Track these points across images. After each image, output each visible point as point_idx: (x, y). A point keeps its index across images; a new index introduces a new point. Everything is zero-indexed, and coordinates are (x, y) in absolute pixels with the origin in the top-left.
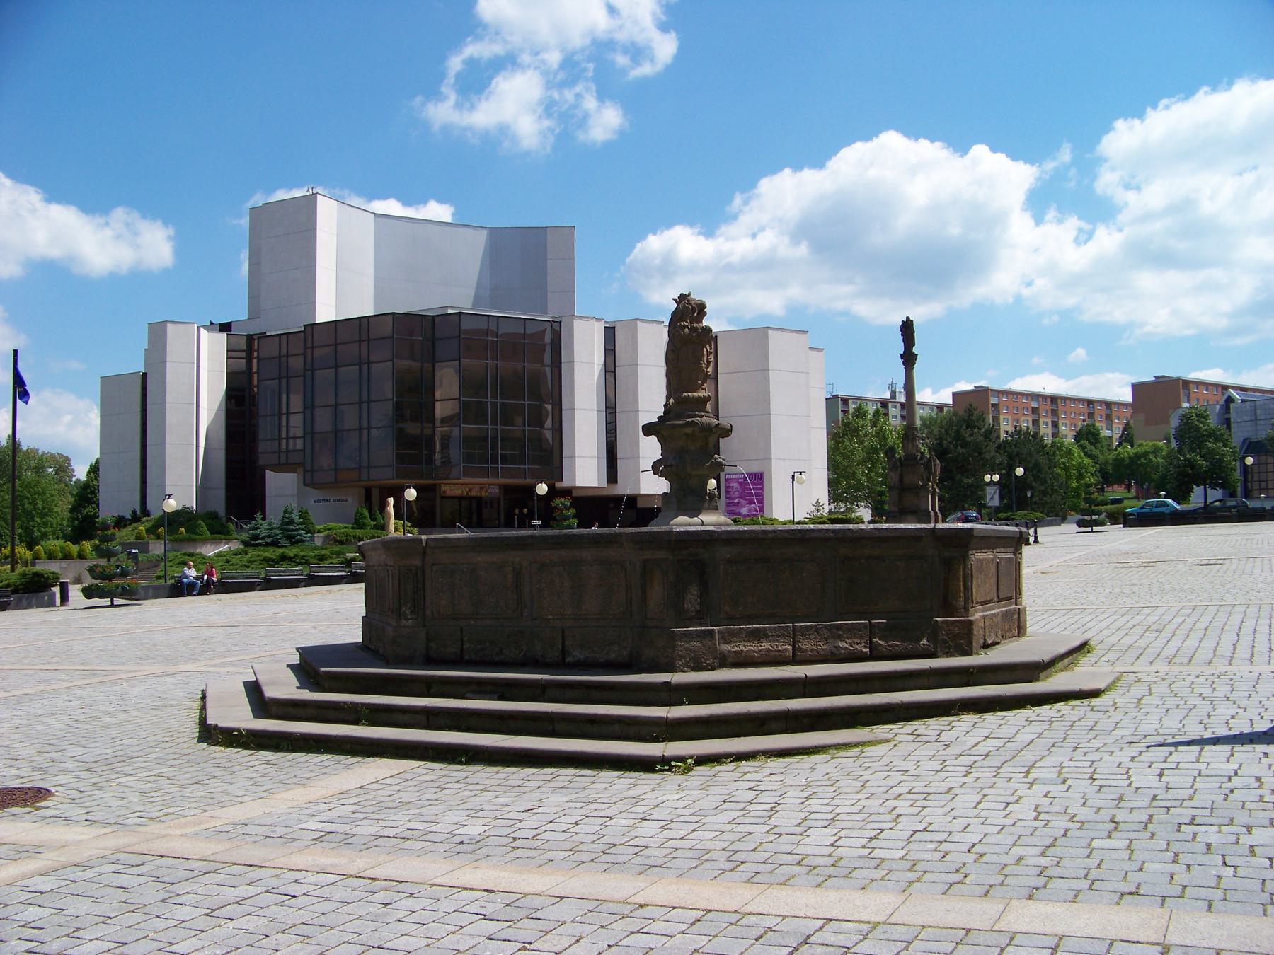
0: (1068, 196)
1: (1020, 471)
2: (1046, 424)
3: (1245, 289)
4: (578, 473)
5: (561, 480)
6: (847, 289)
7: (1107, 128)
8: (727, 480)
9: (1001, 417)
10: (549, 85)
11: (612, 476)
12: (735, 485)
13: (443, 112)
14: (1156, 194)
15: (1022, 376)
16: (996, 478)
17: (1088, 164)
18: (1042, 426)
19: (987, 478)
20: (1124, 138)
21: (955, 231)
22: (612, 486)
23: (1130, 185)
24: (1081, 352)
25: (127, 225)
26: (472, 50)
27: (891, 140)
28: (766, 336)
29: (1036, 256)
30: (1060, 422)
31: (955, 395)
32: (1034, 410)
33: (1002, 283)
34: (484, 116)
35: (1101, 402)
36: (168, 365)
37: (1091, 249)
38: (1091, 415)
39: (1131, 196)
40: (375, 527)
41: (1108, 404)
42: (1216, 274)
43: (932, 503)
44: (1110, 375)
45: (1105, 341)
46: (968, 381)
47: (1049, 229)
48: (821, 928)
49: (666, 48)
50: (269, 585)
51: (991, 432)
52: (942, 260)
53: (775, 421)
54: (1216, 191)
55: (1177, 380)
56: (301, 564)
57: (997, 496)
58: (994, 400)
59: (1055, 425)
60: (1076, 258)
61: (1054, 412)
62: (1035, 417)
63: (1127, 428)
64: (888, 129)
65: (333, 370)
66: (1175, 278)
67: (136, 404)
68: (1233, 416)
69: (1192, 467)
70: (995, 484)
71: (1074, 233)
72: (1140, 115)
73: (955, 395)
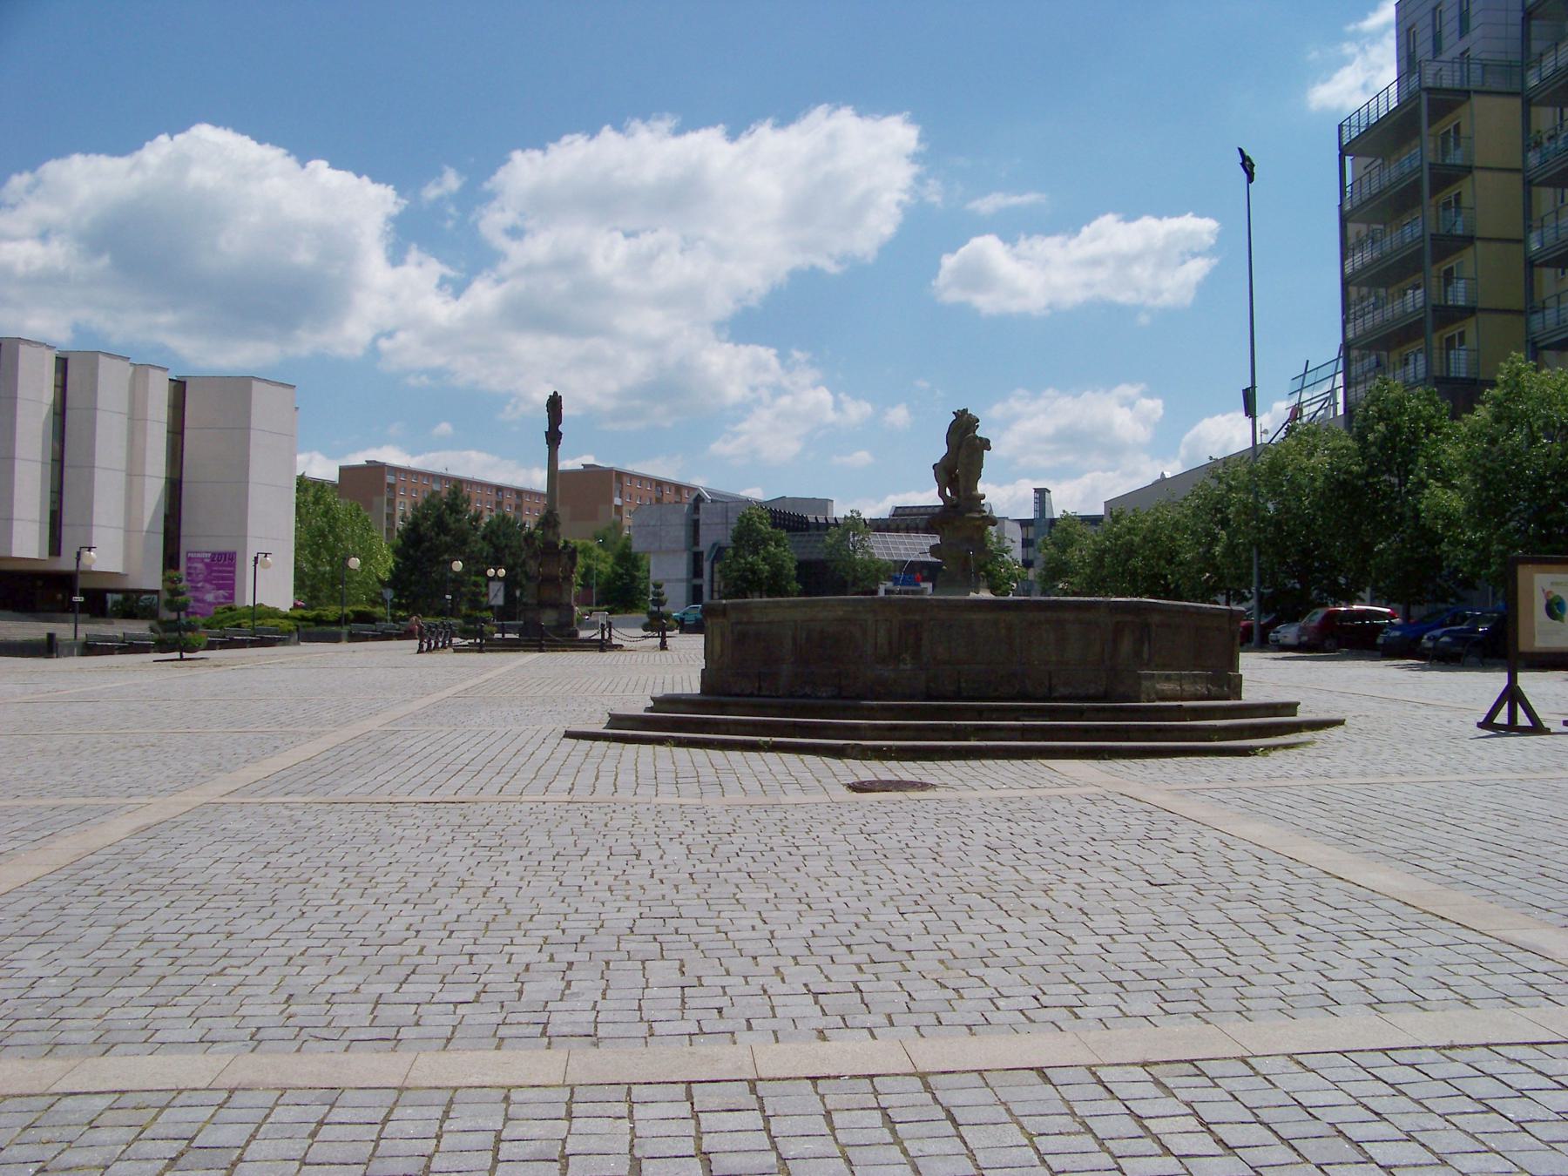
0: (440, 234)
1: (458, 566)
3: (637, 365)
4: (16, 542)
6: (165, 318)
7: (504, 160)
8: (189, 559)
11: (55, 546)
12: (200, 566)
14: (538, 247)
15: (379, 446)
16: (502, 573)
17: (475, 196)
18: (626, 516)
19: (491, 572)
20: (526, 170)
21: (304, 257)
22: (55, 558)
23: (515, 233)
24: (445, 428)
29: (397, 302)
31: (342, 469)
38: (499, 504)
39: (512, 248)
41: (519, 493)
43: (1366, 595)
44: (473, 454)
45: (474, 411)
46: (331, 455)
47: (410, 271)
48: (155, 1119)
52: (289, 294)
53: (254, 491)
54: (608, 253)
55: (610, 470)
57: (501, 595)
58: (390, 479)
60: (442, 311)
66: (554, 343)
68: (702, 517)
69: (754, 572)
70: (500, 579)
71: (436, 281)
73: (342, 469)
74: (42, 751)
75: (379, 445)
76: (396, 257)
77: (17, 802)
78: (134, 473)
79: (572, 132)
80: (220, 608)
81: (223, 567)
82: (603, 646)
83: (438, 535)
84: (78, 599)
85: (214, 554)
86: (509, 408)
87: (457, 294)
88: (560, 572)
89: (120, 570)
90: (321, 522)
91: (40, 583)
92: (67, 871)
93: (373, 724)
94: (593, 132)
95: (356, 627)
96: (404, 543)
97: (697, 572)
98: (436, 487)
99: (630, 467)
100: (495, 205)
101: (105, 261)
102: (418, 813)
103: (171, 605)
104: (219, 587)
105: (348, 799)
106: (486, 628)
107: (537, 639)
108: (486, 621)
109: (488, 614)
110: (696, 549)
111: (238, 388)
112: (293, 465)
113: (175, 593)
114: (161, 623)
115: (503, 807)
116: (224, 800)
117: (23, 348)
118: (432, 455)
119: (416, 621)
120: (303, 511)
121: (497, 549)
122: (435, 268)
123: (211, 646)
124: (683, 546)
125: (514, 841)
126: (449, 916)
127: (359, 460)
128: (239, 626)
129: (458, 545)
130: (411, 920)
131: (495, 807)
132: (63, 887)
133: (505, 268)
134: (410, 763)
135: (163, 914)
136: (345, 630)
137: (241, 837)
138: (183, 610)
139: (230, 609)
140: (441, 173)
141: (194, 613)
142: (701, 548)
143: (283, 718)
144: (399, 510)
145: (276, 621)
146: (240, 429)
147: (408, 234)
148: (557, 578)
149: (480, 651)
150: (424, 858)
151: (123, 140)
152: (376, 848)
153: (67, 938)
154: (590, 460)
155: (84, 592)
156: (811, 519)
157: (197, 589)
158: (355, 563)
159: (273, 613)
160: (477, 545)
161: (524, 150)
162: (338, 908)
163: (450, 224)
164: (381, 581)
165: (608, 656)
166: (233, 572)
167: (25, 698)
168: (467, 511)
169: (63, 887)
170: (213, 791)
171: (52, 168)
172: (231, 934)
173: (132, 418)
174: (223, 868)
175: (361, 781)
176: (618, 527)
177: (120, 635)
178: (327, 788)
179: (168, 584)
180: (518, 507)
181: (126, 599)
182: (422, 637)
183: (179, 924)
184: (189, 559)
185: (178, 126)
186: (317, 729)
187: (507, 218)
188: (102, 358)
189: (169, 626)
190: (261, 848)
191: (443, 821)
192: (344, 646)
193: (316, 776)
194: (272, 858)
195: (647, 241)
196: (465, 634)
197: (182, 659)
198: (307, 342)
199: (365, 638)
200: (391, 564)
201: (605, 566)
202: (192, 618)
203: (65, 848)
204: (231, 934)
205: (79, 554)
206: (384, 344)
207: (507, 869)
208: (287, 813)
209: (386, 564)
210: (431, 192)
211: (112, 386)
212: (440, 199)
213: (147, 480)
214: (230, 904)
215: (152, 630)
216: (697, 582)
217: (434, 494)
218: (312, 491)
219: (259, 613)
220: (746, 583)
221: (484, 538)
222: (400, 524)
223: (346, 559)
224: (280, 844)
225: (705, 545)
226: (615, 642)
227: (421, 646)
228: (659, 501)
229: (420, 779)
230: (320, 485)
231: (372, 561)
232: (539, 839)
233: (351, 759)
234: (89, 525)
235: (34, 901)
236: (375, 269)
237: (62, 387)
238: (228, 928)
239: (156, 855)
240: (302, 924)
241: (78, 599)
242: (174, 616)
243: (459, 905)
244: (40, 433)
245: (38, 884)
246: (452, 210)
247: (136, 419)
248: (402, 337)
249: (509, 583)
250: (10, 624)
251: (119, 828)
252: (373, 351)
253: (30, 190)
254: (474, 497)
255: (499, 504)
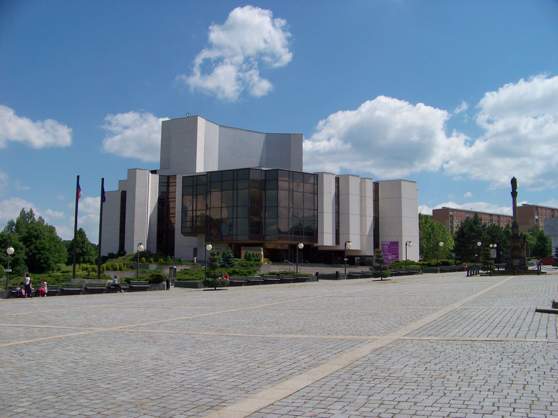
1: (479, 244)
3: (540, 166)
5: (317, 242)
6: (369, 163)
7: (483, 96)
8: (382, 245)
9: (454, 221)
10: (240, 70)
13: (196, 80)
14: (500, 126)
17: (474, 110)
18: (540, 223)
19: (491, 246)
20: (490, 99)
21: (415, 138)
23: (490, 122)
24: (469, 194)
25: (52, 127)
26: (206, 54)
27: (382, 99)
28: (400, 184)
29: (449, 150)
33: (435, 162)
34: (210, 83)
35: (495, 215)
36: (137, 188)
37: (473, 149)
38: (491, 221)
39: (490, 127)
40: (255, 260)
41: (499, 216)
42: (527, 160)
44: (481, 203)
45: (480, 188)
46: (429, 206)
49: (287, 57)
50: (232, 284)
51: (54, 239)
52: (412, 150)
53: (404, 220)
54: (526, 125)
55: (533, 206)
56: (241, 275)
57: (495, 254)
58: (451, 213)
60: (465, 152)
64: (381, 95)
65: (232, 191)
66: (508, 160)
67: (120, 204)
71: (464, 142)
72: (497, 90)
73: (433, 210)
74: (337, 316)
75: (447, 202)
76: (449, 135)
77: (329, 336)
78: (362, 215)
79: (508, 83)
80: (394, 261)
81: (394, 247)
82: (538, 272)
83: (471, 232)
84: (346, 259)
85: (391, 242)
86: (491, 186)
87: (471, 146)
88: (519, 244)
89: (359, 249)
90: (430, 230)
91: (333, 254)
92: (348, 368)
93: (457, 305)
94: (516, 82)
95: (443, 267)
96: (458, 236)
98: (468, 215)
99: (540, 204)
100: (481, 112)
101: (349, 145)
102: (484, 346)
103: (377, 261)
104: (393, 254)
105: (454, 338)
106: (492, 267)
107: (512, 270)
108: (490, 264)
109: (492, 262)
111: (397, 184)
112: (417, 209)
113: (379, 257)
114: (374, 267)
115: (519, 344)
116: (405, 338)
117: (325, 175)
118: (467, 204)
119: (466, 265)
120: (421, 226)
121: (492, 237)
122: (463, 137)
123: (392, 275)
125: (530, 361)
126: (510, 400)
127: (439, 207)
128: (401, 268)
129: (478, 236)
130: (493, 400)
131: (516, 344)
132: (347, 375)
133: (487, 135)
134: (475, 322)
135: (387, 391)
136: (439, 268)
137: (414, 355)
138: (381, 263)
139: (398, 262)
140: (461, 104)
141: (385, 264)
143: (422, 303)
144: (455, 224)
145: (414, 266)
146: (398, 198)
147: (451, 127)
148: (519, 247)
149: (490, 275)
150: (492, 368)
151: (353, 105)
152: (470, 362)
153: (351, 400)
154: (525, 203)
155: (347, 257)
157: (385, 255)
158: (441, 244)
159: (413, 263)
160: (485, 235)
161: (490, 92)
162: (459, 392)
163: (466, 120)
164: (450, 250)
165: (541, 277)
166: (398, 249)
167: (330, 295)
168: (481, 223)
169: (347, 375)
170: (400, 334)
171: (332, 117)
172: (416, 403)
173: (361, 197)
174: (408, 369)
175: (457, 330)
176: (537, 227)
177: (360, 272)
178: (445, 333)
179: (376, 254)
180: (499, 221)
181: (361, 259)
182: (468, 270)
183: (394, 396)
184: (382, 245)
185: (372, 98)
186: (435, 308)
187: (486, 117)
188: (350, 176)
189: (377, 268)
190: (423, 361)
191: (495, 350)
192: (439, 274)
193: (439, 328)
194: (428, 365)
195: (541, 119)
196: (484, 269)
197: (382, 280)
198: (419, 167)
199: (446, 271)
200: (453, 244)
201: (532, 241)
202: (385, 265)
203: (347, 357)
204: (416, 403)
205: (346, 244)
206: (445, 166)
207: (530, 375)
208: (430, 344)
209: (452, 244)
210: (457, 111)
211: (354, 186)
212: (461, 112)
213: (367, 217)
214: (414, 387)
215: (371, 269)
217: (468, 218)
218: (424, 219)
219: (408, 263)
221: (488, 233)
222: (455, 230)
223: (438, 243)
224: (430, 358)
226: (542, 271)
227: (468, 274)
228: (553, 216)
229: (481, 330)
230: (426, 217)
231: (447, 243)
232: (540, 361)
233: (451, 321)
234: (348, 234)
235: (337, 381)
236: (441, 138)
237: (338, 187)
238: (414, 400)
239: (381, 362)
240: (445, 400)
241: (346, 259)
242: (378, 265)
243: (514, 395)
244: (331, 203)
245: (338, 373)
246: (466, 115)
247: (362, 197)
248: (451, 163)
249: (498, 249)
250: (324, 268)
251: (366, 350)
252: (442, 169)
253: (324, 125)
254: (483, 218)
255: (491, 221)
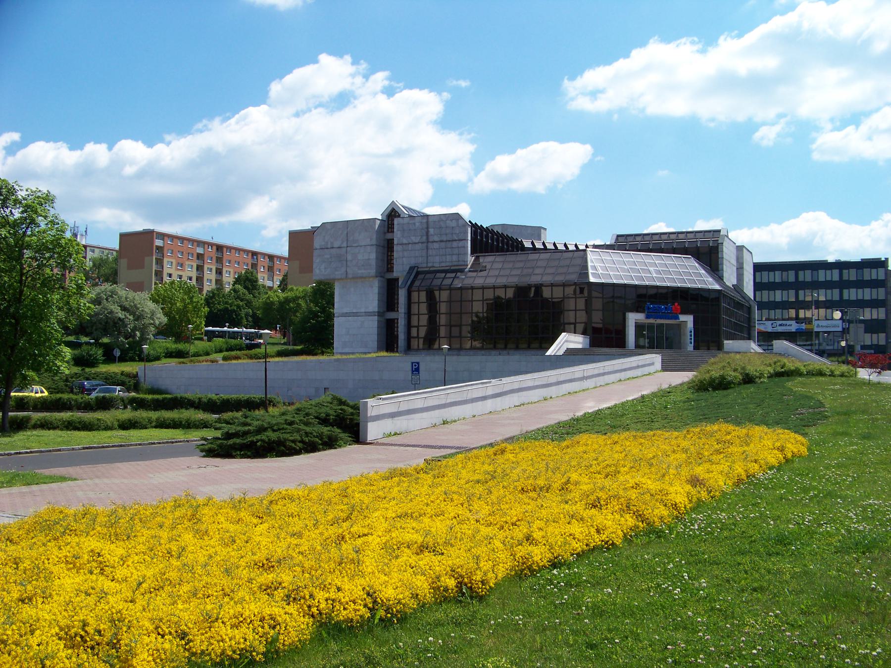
2: (211, 270)
30: (224, 270)
32: (200, 256)
35: (264, 255)
38: (254, 266)
41: (271, 257)
58: (158, 243)
59: (219, 272)
61: (219, 260)
62: (200, 263)
63: (285, 277)
68: (397, 236)
97: (389, 300)
110: (389, 276)
124: (373, 272)
142: (395, 274)
156: (527, 244)
216: (391, 315)
220: (322, 640)
225: (400, 271)
